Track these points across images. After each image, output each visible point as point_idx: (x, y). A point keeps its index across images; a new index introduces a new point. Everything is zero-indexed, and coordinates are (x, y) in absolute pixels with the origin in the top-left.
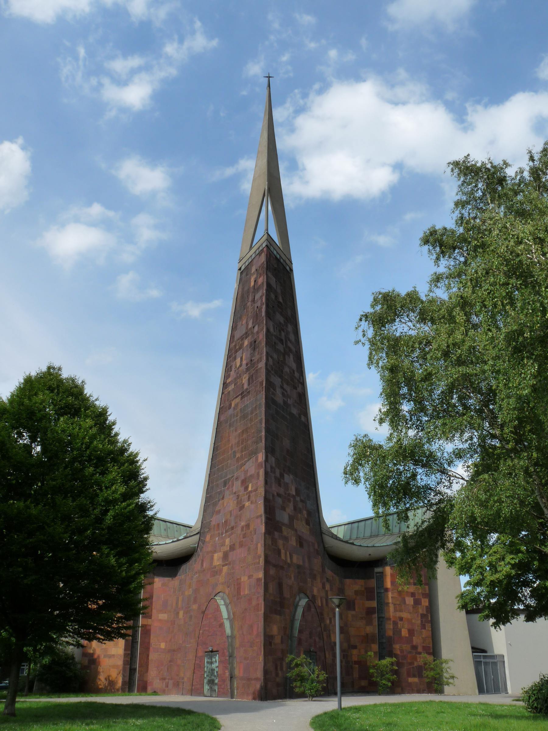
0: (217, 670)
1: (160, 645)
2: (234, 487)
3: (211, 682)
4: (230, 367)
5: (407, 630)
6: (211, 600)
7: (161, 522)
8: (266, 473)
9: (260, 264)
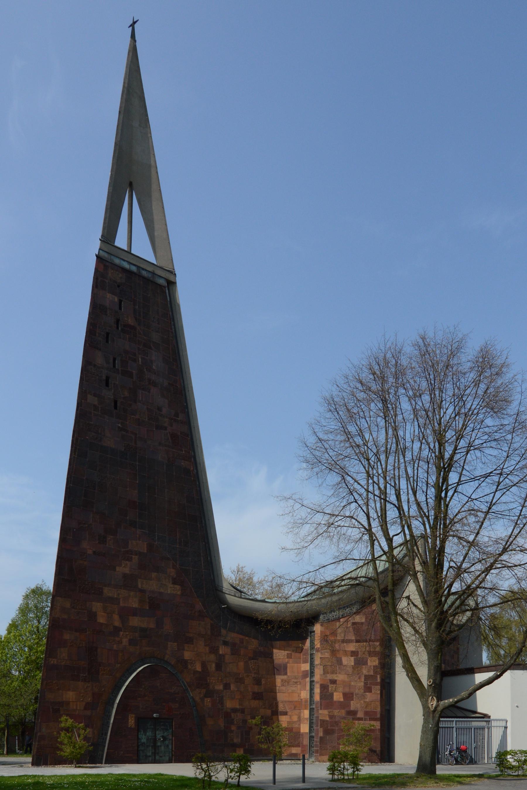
5: (342, 694)
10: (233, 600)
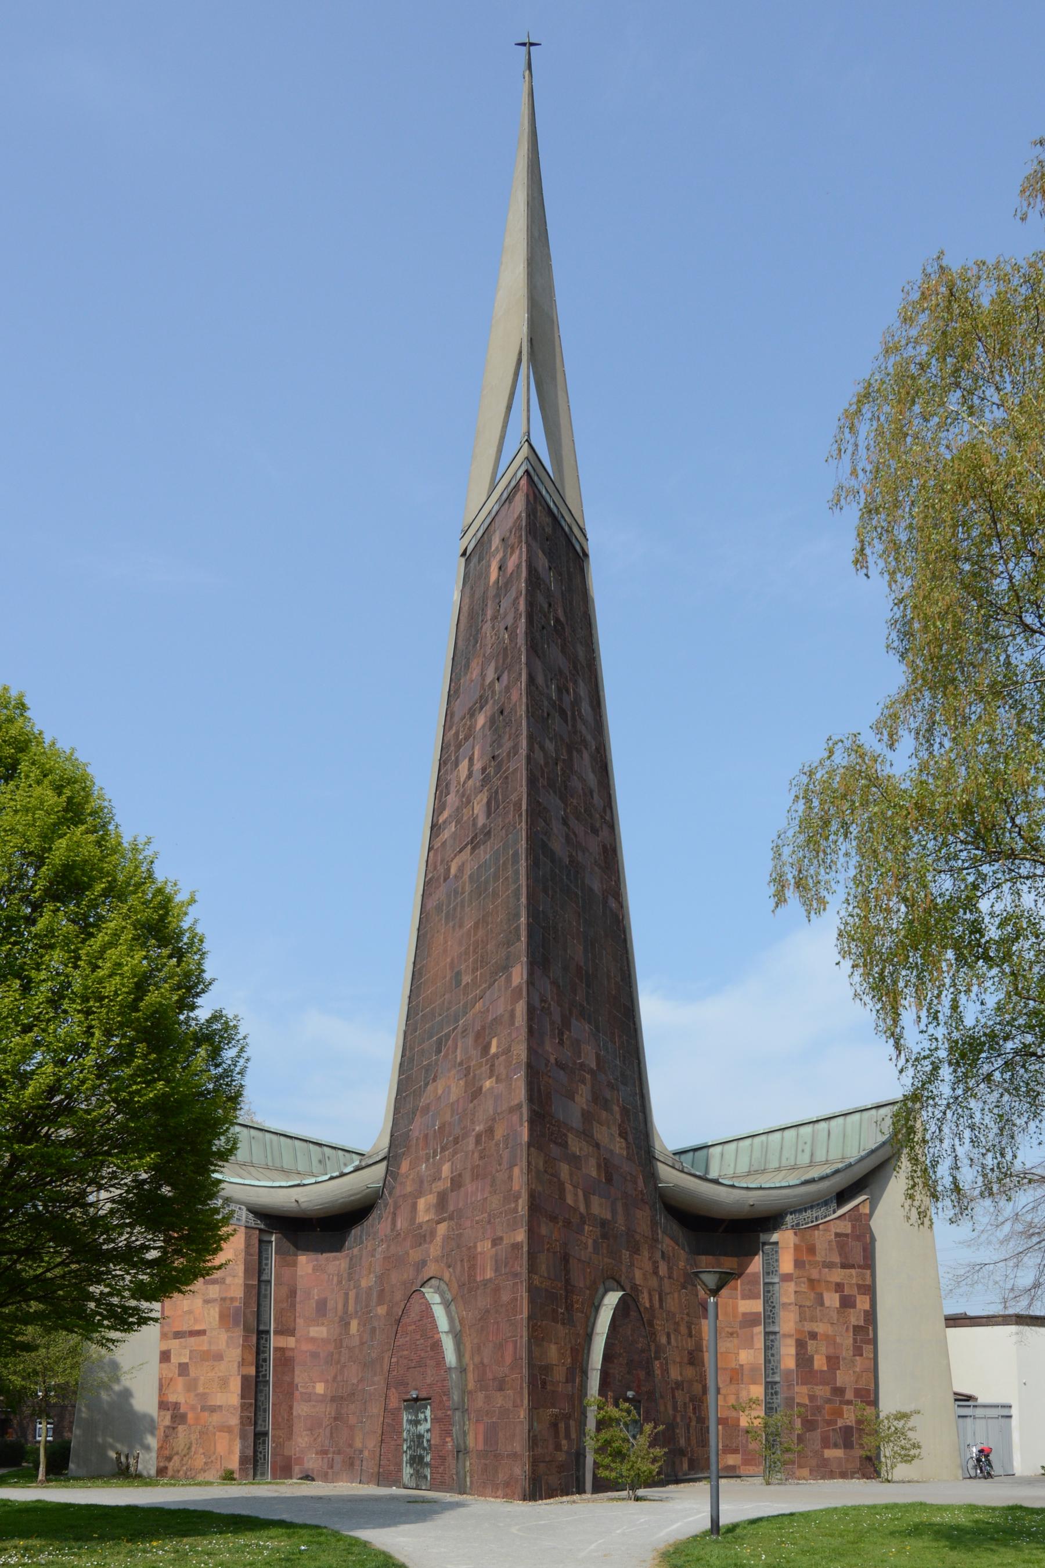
0: (427, 1436)
1: (314, 1387)
2: (459, 1051)
3: (417, 1461)
4: (447, 785)
6: (414, 1293)
7: (311, 1145)
8: (531, 1011)
9: (510, 523)
10: (668, 1176)
